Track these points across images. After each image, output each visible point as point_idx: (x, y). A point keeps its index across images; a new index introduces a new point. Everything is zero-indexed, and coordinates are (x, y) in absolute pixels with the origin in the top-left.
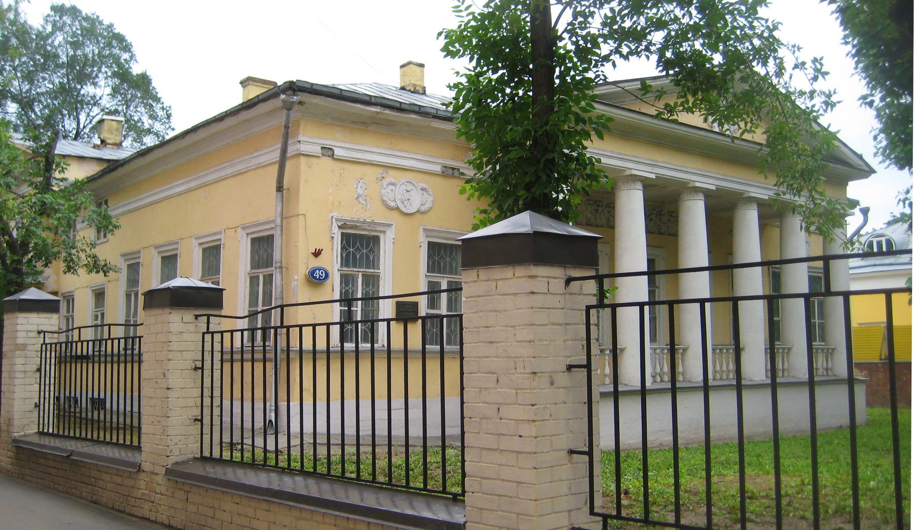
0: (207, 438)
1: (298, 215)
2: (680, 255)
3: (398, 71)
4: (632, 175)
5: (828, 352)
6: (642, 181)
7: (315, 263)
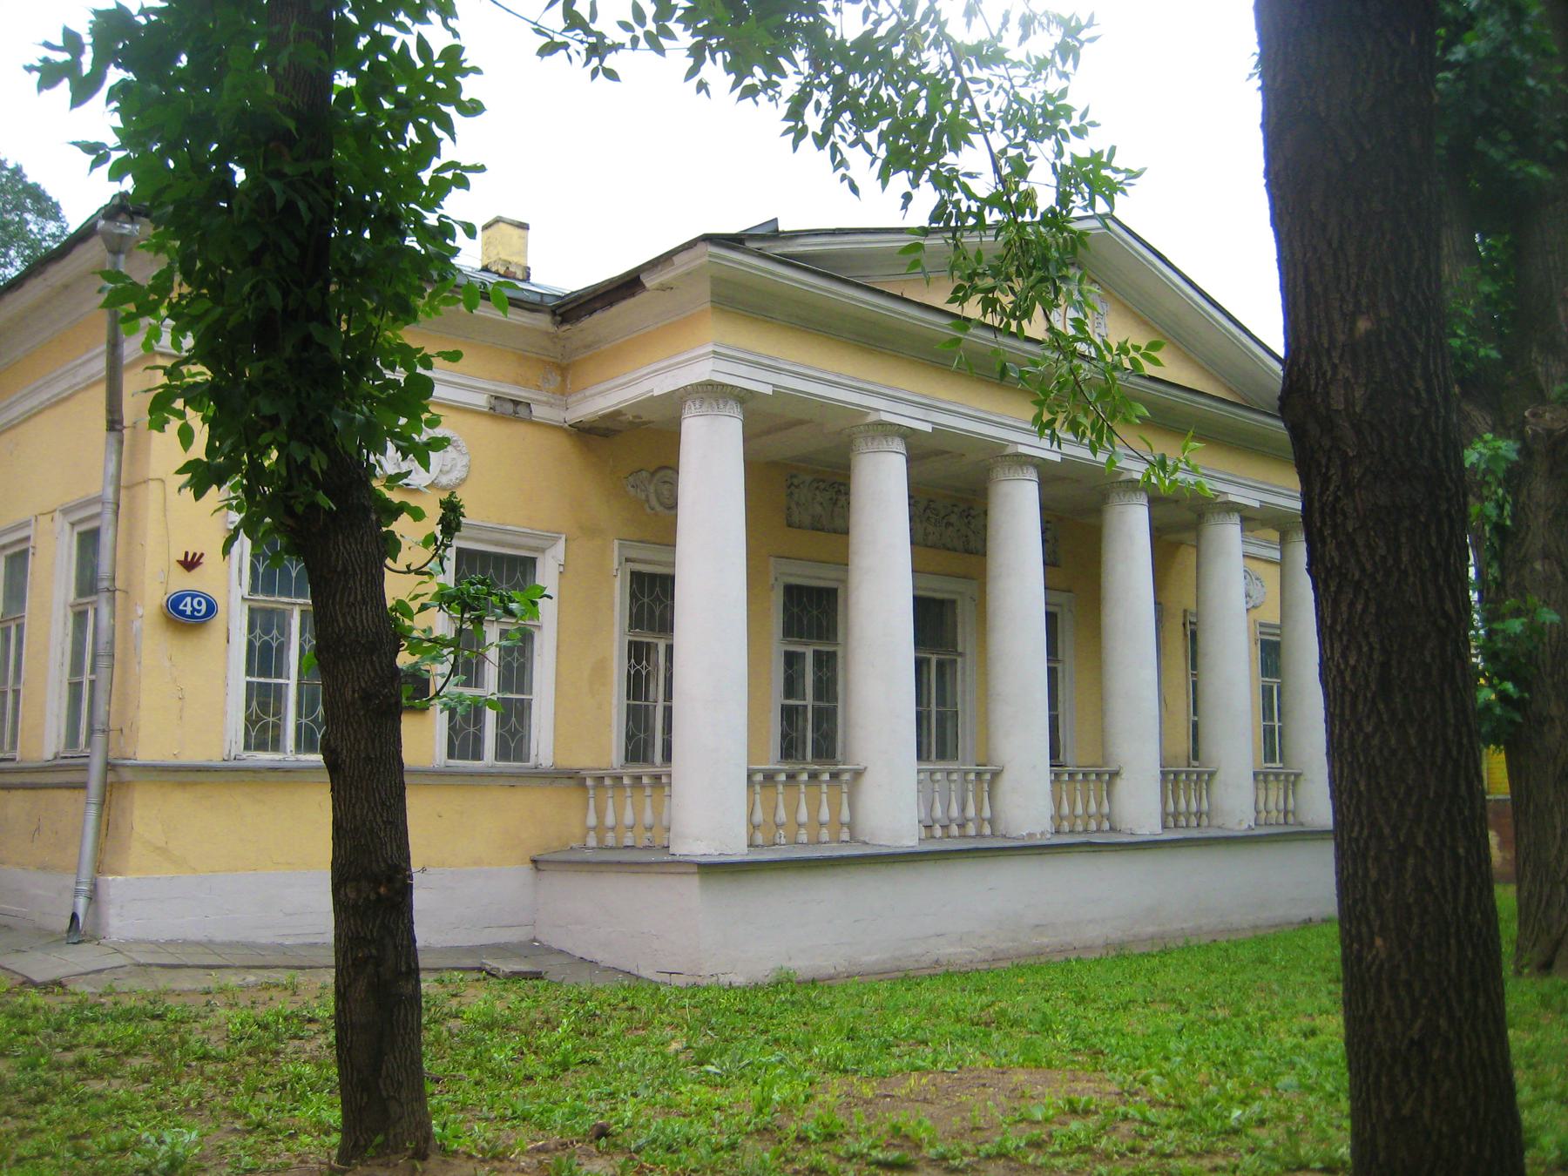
1: (146, 482)
4: (1019, 455)
5: (1287, 780)
6: (1036, 466)
7: (184, 581)
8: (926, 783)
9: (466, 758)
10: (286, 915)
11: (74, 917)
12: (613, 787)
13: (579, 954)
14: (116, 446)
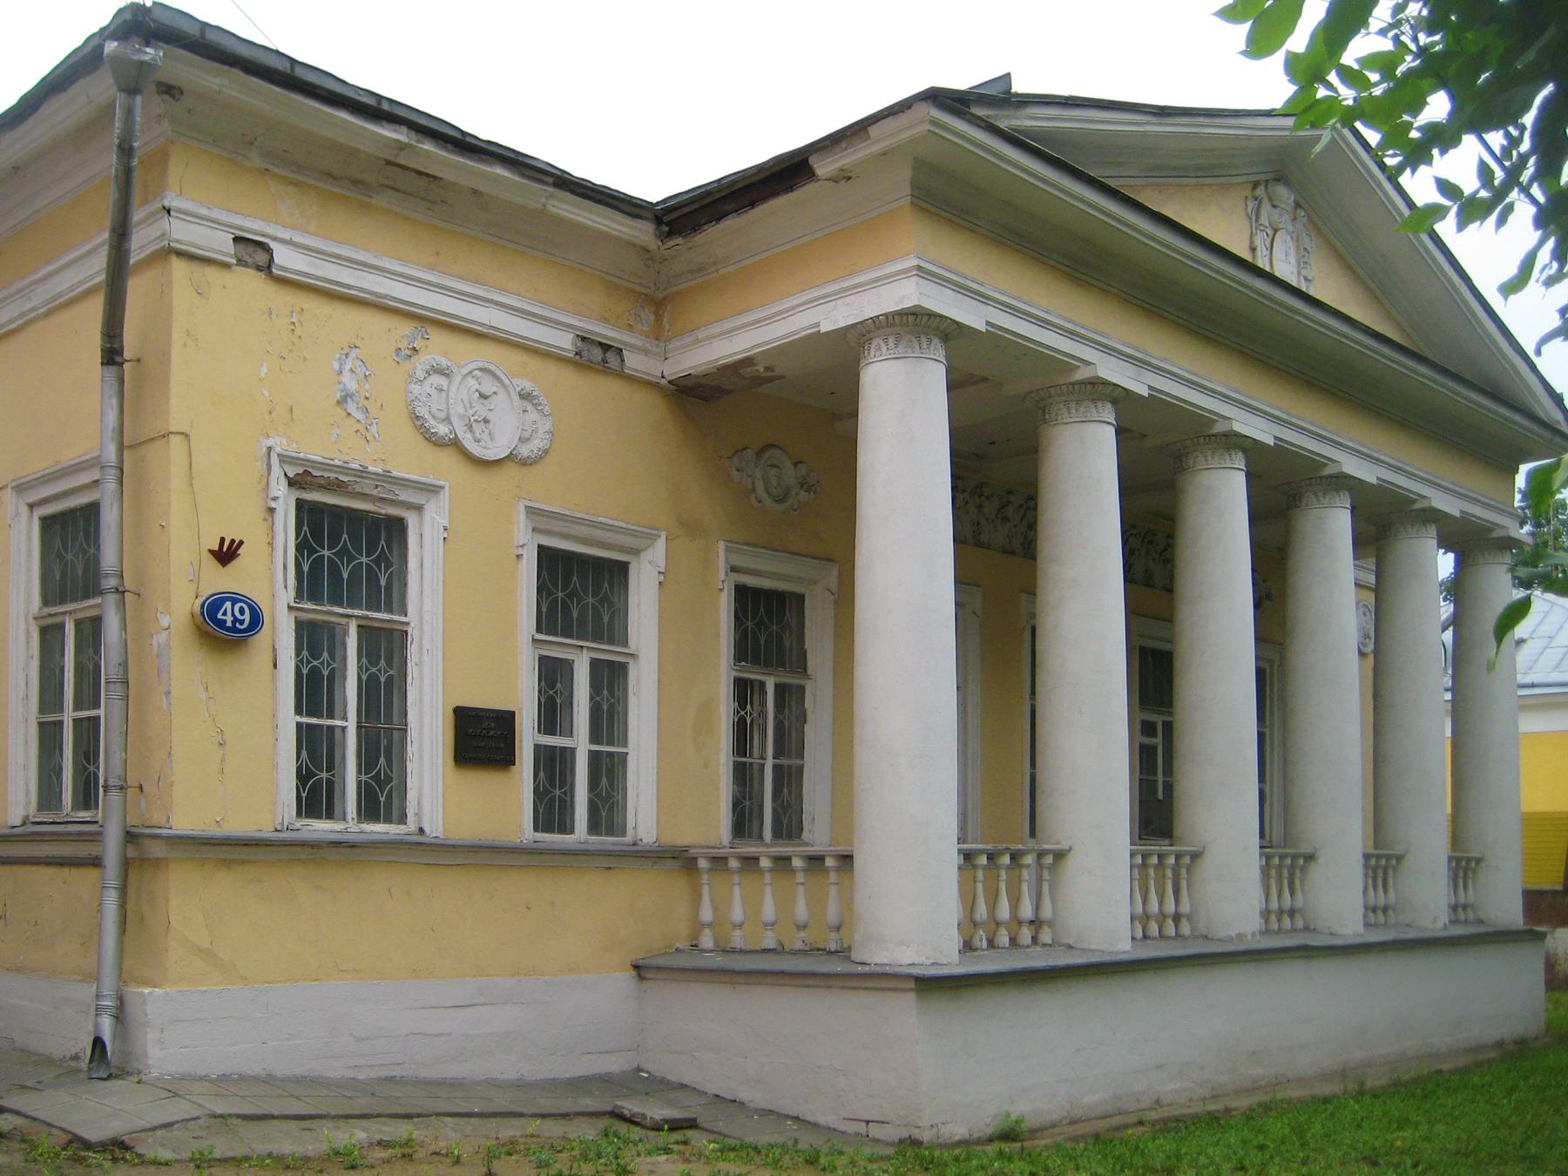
8: (1140, 868)
9: (552, 831)
10: (359, 1040)
11: (98, 1043)
12: (741, 870)
13: (712, 1089)
14: (112, 390)
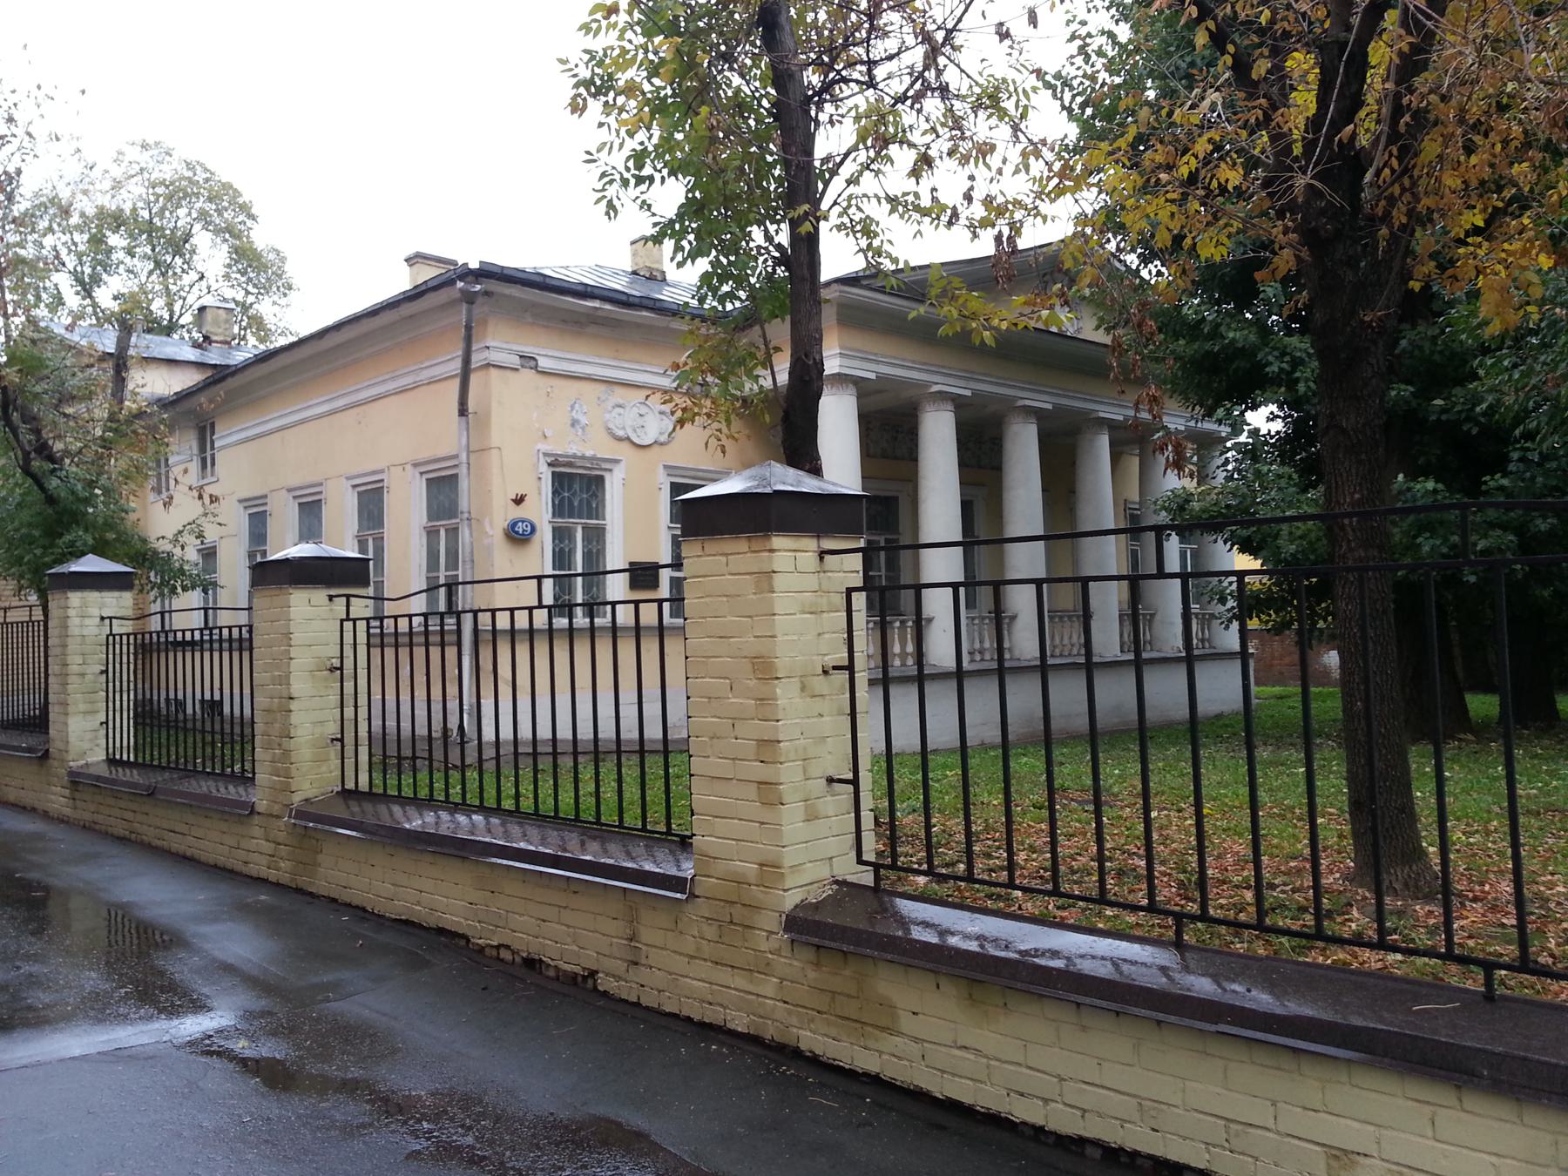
0: (349, 762)
2: (1005, 496)
3: (628, 249)
14: (464, 425)
